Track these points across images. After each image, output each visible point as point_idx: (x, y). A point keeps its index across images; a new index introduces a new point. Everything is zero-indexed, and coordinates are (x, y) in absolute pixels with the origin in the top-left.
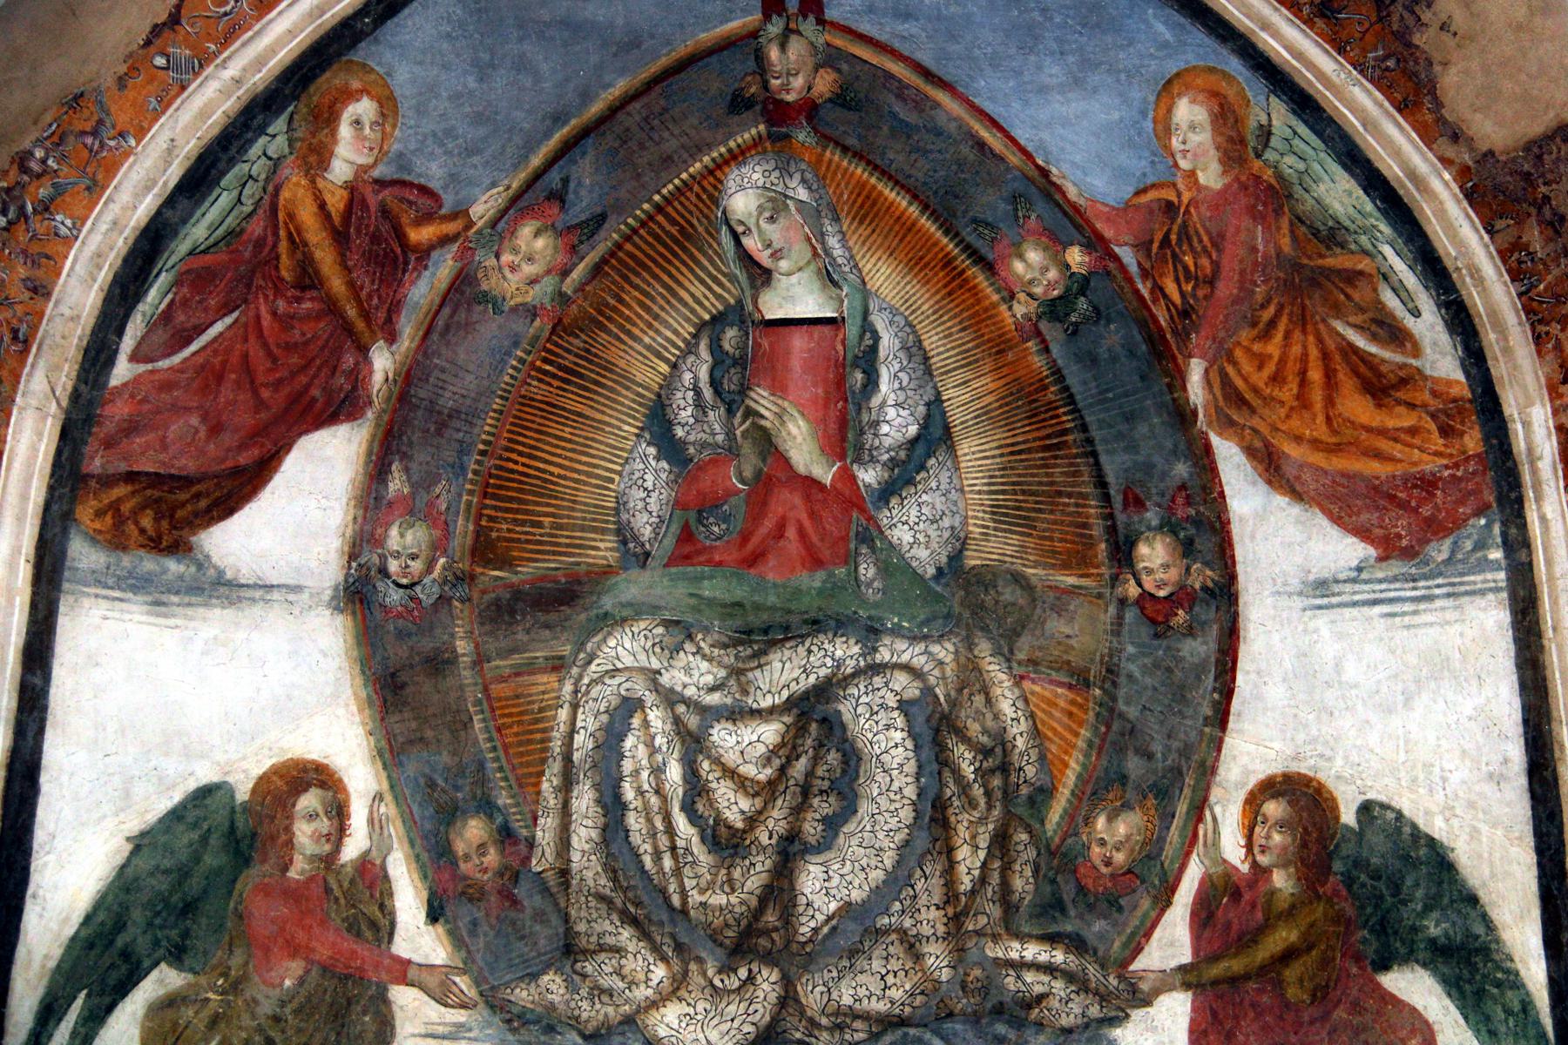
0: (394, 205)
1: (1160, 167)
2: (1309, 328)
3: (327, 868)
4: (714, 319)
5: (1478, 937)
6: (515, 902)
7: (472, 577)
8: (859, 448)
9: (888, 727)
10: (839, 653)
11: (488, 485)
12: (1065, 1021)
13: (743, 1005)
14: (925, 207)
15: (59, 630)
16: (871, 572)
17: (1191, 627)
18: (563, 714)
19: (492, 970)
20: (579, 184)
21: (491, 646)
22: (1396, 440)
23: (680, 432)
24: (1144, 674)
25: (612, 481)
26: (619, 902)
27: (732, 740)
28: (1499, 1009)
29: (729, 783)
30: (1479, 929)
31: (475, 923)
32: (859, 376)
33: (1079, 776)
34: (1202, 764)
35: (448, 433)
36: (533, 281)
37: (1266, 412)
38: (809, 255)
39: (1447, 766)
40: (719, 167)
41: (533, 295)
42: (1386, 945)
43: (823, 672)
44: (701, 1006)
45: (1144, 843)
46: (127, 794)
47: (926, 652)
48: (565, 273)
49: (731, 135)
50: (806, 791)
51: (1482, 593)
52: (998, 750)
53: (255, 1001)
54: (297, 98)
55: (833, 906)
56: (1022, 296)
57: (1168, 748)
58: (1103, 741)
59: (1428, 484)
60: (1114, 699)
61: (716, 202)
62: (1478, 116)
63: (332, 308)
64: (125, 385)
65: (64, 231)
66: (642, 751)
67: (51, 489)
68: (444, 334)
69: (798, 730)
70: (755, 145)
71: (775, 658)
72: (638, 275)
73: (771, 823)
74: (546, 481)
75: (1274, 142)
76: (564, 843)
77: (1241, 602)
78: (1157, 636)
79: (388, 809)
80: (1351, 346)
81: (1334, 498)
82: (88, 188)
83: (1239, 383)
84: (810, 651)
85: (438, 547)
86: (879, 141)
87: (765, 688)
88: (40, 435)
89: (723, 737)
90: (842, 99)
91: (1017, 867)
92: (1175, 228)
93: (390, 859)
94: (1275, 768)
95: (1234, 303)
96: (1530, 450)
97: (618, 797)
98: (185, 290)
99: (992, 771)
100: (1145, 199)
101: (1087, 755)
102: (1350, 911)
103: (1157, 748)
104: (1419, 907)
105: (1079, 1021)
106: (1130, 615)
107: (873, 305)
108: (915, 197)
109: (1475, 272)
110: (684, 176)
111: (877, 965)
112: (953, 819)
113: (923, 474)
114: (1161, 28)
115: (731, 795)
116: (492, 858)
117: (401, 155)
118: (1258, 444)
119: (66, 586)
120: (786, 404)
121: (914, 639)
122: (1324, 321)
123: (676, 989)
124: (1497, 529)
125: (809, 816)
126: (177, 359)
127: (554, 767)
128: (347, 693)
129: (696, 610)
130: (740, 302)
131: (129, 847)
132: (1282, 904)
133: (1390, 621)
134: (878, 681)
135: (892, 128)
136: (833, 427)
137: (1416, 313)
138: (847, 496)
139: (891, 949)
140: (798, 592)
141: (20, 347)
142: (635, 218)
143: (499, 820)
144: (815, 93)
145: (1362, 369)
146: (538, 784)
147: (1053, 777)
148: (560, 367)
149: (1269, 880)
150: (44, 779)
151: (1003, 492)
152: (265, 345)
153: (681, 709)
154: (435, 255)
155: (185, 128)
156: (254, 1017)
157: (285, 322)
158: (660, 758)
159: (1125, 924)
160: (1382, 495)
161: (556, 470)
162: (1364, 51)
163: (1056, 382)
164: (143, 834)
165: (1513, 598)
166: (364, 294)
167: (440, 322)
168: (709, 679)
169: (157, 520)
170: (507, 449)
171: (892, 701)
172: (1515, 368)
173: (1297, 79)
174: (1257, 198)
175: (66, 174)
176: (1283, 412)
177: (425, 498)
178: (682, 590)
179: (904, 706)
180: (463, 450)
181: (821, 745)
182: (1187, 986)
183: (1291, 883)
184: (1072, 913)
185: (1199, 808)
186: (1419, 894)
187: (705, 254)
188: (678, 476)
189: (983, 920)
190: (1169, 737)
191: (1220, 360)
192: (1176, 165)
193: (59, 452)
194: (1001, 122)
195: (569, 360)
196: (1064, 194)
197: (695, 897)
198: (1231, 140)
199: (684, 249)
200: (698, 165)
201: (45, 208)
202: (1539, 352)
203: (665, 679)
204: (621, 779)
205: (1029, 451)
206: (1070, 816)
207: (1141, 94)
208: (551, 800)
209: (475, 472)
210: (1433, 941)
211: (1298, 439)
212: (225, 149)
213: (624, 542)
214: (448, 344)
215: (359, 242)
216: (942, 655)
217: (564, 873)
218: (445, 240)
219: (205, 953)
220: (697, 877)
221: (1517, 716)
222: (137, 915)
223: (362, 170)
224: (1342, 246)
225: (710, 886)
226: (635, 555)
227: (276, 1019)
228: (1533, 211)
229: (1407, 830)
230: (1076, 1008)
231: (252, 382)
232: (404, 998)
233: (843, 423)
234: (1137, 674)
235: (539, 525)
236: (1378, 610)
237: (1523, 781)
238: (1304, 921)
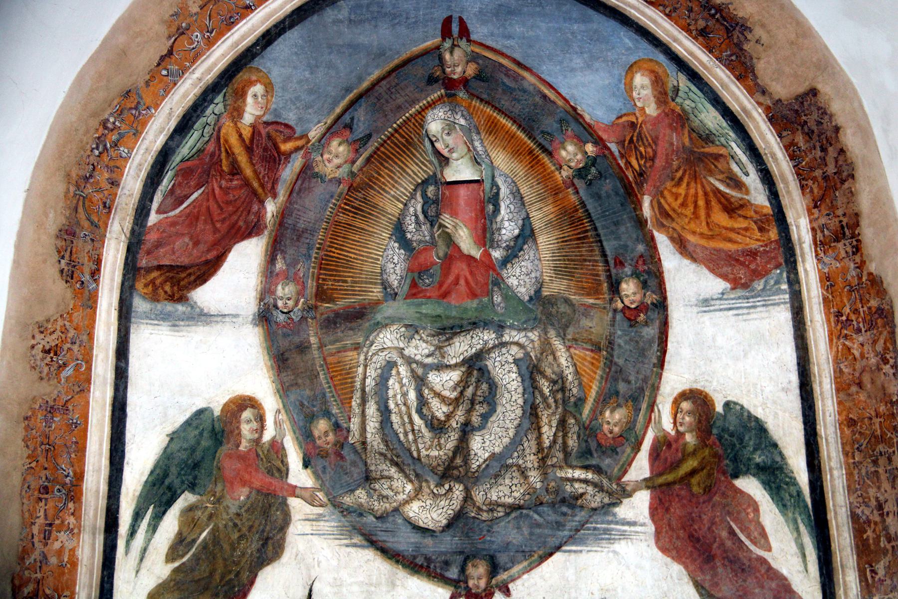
0: (273, 134)
1: (628, 106)
2: (698, 181)
3: (257, 445)
4: (423, 182)
5: (777, 462)
6: (342, 458)
7: (316, 307)
8: (492, 240)
9: (509, 372)
10: (486, 338)
11: (321, 264)
12: (594, 505)
13: (448, 501)
14: (520, 126)
15: (131, 341)
16: (499, 300)
17: (646, 322)
18: (360, 370)
19: (333, 488)
20: (359, 120)
21: (326, 339)
22: (738, 233)
23: (409, 236)
24: (625, 344)
25: (378, 260)
26: (389, 456)
27: (438, 379)
28: (787, 495)
29: (437, 399)
30: (778, 459)
31: (324, 468)
32: (491, 207)
33: (597, 392)
34: (653, 385)
35: (303, 240)
36: (339, 167)
37: (679, 220)
38: (466, 150)
39: (764, 384)
40: (423, 110)
41: (339, 174)
42: (737, 467)
43: (479, 347)
44: (428, 502)
45: (627, 423)
46: (165, 415)
47: (526, 336)
48: (353, 162)
49: (428, 95)
50: (473, 402)
51: (778, 304)
52: (560, 381)
53: (228, 507)
54: (227, 86)
55: (487, 455)
56: (565, 167)
57: (637, 378)
58: (608, 375)
59: (753, 254)
60: (612, 356)
61: (422, 127)
62: (774, 83)
63: (247, 183)
64: (154, 225)
65: (124, 155)
66: (397, 386)
67: (124, 275)
68: (298, 193)
69: (469, 374)
70: (440, 99)
71: (457, 341)
72: (387, 162)
73: (457, 418)
74: (348, 261)
75: (680, 94)
76: (363, 429)
77: (669, 309)
78: (631, 326)
79: (283, 416)
80: (717, 189)
81: (711, 260)
82: (134, 134)
83: (667, 207)
84: (472, 337)
85: (300, 293)
86: (497, 96)
87: (452, 355)
88: (118, 250)
89: (434, 378)
90: (480, 76)
91: (570, 435)
92: (636, 134)
93: (285, 440)
94: (686, 387)
95: (664, 169)
96: (799, 239)
97: (387, 407)
98: (180, 178)
99: (558, 391)
100: (621, 121)
101: (600, 383)
102: (720, 452)
103: (632, 378)
104: (751, 449)
105: (600, 505)
106: (619, 317)
107: (497, 173)
108: (515, 122)
109: (773, 155)
110: (407, 115)
111: (507, 481)
112: (540, 414)
113: (522, 253)
114: (627, 41)
115: (438, 404)
116: (331, 437)
117: (275, 110)
118: (675, 235)
119: (133, 320)
120: (457, 221)
121: (520, 330)
122: (705, 177)
123: (417, 494)
124: (785, 275)
125: (475, 413)
126: (177, 211)
127: (357, 395)
128: (262, 364)
129: (420, 319)
130: (435, 174)
131: (168, 439)
132: (690, 449)
133: (737, 317)
134: (504, 350)
135: (503, 90)
136: (480, 232)
137: (747, 174)
138: (487, 264)
139: (514, 474)
140: (466, 310)
141: (107, 210)
142: (385, 135)
143: (334, 420)
144: (467, 74)
145: (723, 200)
146: (350, 403)
147: (585, 393)
148: (353, 207)
149: (684, 438)
150: (129, 410)
151: (559, 260)
152: (217, 202)
153: (414, 366)
154: (293, 156)
155: (177, 103)
156: (228, 514)
157: (226, 191)
158: (405, 389)
159: (619, 460)
160: (732, 259)
161: (353, 256)
162: (721, 52)
163: (582, 208)
164: (174, 433)
165: (792, 307)
166: (261, 176)
167: (297, 187)
168: (426, 351)
169: (172, 287)
170: (330, 246)
171: (511, 360)
172: (793, 200)
173: (691, 65)
174: (673, 120)
175: (124, 128)
176: (687, 220)
177: (293, 271)
178: (412, 310)
179: (516, 362)
180: (310, 248)
181: (479, 381)
182: (648, 487)
183: (694, 439)
184: (595, 455)
185: (652, 406)
186: (751, 443)
187: (418, 151)
188: (409, 256)
189: (555, 460)
190: (638, 373)
191: (658, 195)
192: (635, 105)
193: (127, 258)
194: (554, 86)
195: (357, 204)
196: (584, 120)
197: (424, 453)
198: (660, 93)
199: (408, 149)
200: (413, 110)
201: (115, 145)
202: (803, 194)
203: (406, 352)
204: (388, 399)
205: (570, 240)
206: (593, 411)
207: (619, 71)
208: (356, 410)
209: (316, 258)
210: (758, 465)
211: (694, 233)
212: (195, 111)
213: (385, 289)
214: (301, 197)
215: (258, 151)
216: (533, 337)
217: (364, 443)
218: (297, 149)
219: (205, 486)
220: (424, 443)
221: (795, 361)
222: (174, 470)
223: (259, 117)
224: (713, 142)
225: (430, 447)
226: (391, 294)
227: (238, 515)
228: (800, 128)
229: (746, 414)
230: (598, 498)
231: (212, 220)
232: (294, 503)
233: (484, 230)
234: (622, 344)
235: (346, 282)
236: (731, 312)
237: (797, 391)
238: (700, 456)
